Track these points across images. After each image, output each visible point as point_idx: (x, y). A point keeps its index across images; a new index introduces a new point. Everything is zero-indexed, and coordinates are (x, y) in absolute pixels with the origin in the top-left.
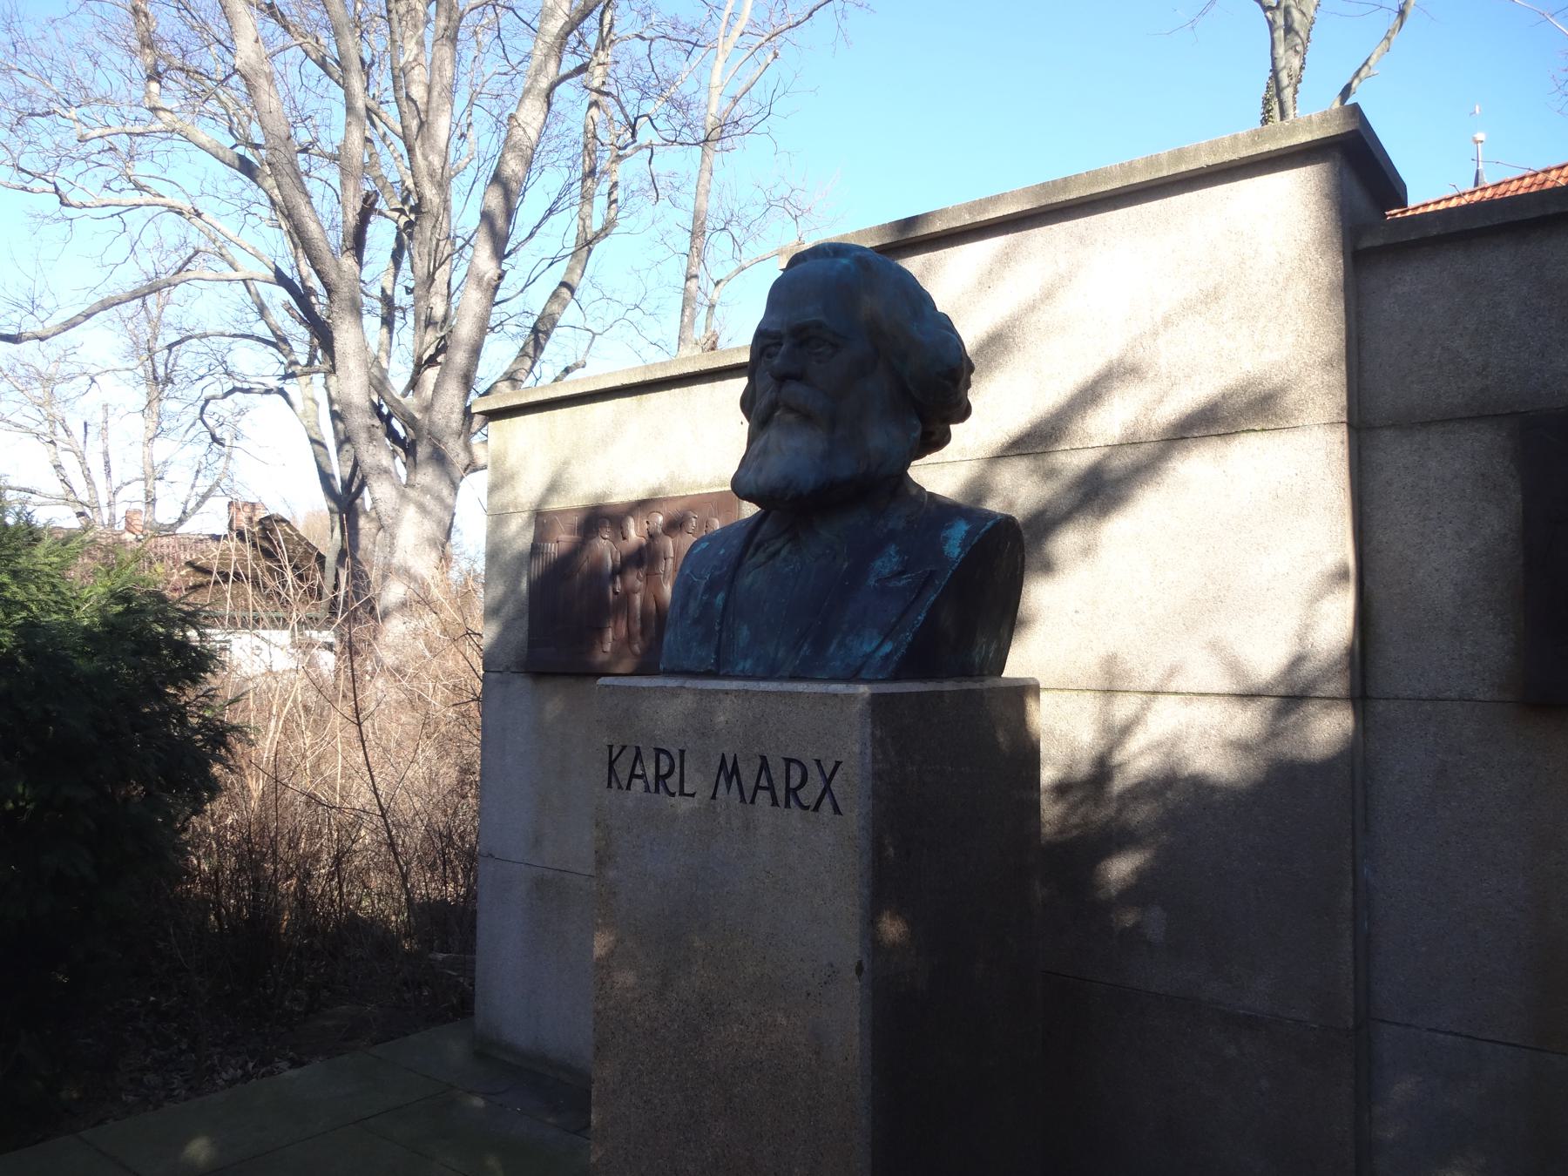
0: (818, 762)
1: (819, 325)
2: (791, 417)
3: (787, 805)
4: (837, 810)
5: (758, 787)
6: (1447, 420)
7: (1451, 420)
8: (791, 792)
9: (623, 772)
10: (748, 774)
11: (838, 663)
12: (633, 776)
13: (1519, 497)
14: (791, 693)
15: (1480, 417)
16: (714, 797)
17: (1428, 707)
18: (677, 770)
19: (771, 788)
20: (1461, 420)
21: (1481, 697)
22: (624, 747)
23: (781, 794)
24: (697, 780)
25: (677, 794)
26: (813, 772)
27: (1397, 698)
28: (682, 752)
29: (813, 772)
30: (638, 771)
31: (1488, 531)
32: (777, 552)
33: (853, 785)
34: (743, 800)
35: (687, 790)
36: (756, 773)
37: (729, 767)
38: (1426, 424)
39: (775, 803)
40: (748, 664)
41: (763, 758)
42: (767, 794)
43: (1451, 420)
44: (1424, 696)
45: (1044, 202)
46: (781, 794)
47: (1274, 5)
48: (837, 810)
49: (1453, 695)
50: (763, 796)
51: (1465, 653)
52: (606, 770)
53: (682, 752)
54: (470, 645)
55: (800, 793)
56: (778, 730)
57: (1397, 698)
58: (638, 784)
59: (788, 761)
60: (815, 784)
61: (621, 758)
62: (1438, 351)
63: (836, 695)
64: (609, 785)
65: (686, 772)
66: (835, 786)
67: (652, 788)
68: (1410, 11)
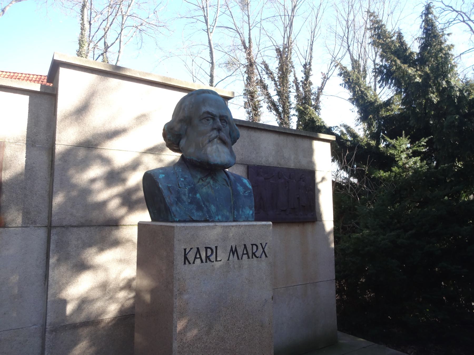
0: (261, 244)
3: (252, 258)
4: (266, 256)
5: (243, 254)
8: (254, 254)
9: (191, 257)
10: (240, 251)
11: (243, 216)
12: (196, 258)
14: (253, 225)
15: (242, 164)
16: (228, 260)
18: (214, 253)
19: (247, 254)
22: (191, 249)
23: (250, 255)
24: (222, 255)
25: (215, 261)
28: (216, 247)
30: (198, 256)
34: (238, 258)
35: (218, 259)
36: (243, 250)
37: (234, 249)
39: (249, 258)
40: (220, 217)
42: (246, 256)
45: (164, 82)
46: (250, 255)
48: (266, 256)
50: (245, 257)
52: (183, 258)
53: (216, 247)
55: (256, 254)
56: (249, 236)
58: (198, 261)
59: (252, 245)
61: (190, 253)
63: (266, 225)
64: (185, 263)
65: (218, 253)
66: (266, 250)
67: (204, 261)
68: (6, 11)
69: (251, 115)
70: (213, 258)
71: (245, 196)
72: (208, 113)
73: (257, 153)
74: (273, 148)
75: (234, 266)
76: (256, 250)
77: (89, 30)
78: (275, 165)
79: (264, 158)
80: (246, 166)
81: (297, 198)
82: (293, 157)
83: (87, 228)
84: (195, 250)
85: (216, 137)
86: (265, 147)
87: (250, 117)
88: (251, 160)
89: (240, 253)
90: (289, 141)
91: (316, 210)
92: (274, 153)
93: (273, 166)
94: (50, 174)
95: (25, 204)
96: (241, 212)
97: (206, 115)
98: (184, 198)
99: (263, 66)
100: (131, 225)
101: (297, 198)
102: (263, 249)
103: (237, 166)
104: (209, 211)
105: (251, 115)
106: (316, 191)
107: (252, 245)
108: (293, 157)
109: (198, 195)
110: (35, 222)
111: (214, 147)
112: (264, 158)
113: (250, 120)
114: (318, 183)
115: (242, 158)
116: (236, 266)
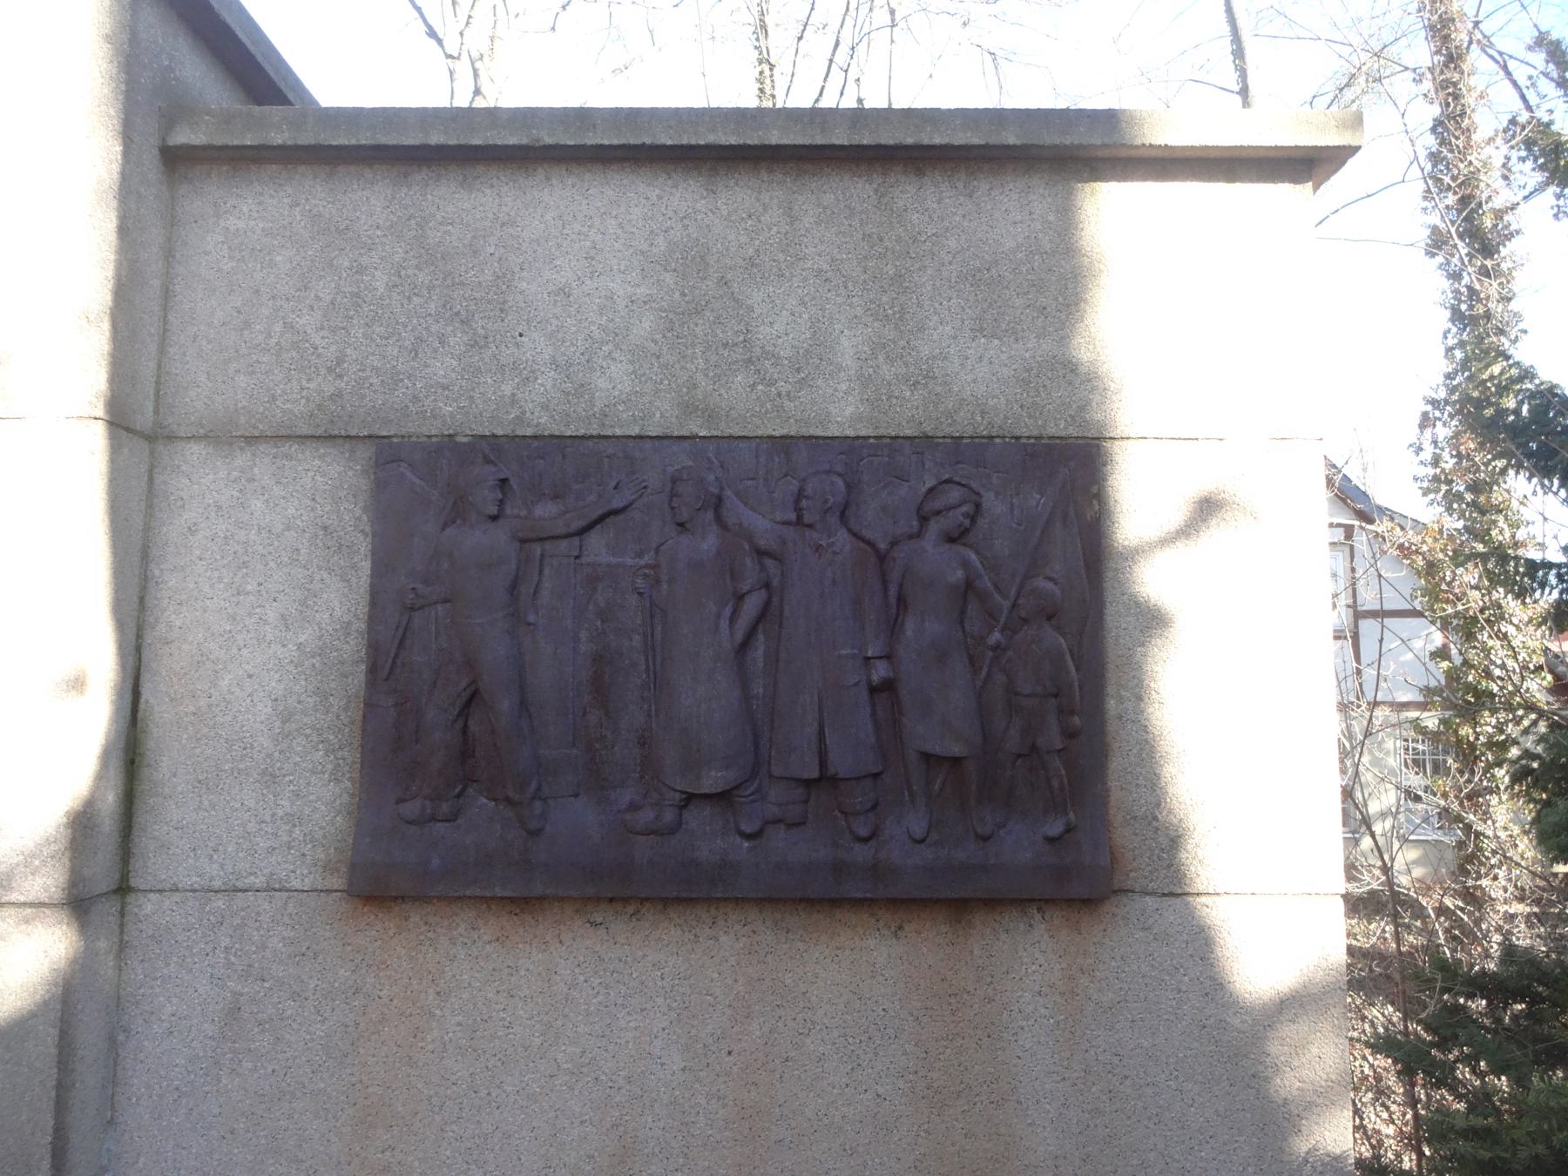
6: (283, 437)
7: (289, 437)
13: (366, 566)
17: (220, 902)
21: (296, 884)
27: (175, 889)
31: (326, 616)
38: (251, 440)
43: (289, 437)
44: (217, 884)
47: (456, 55)
49: (259, 881)
51: (280, 812)
57: (175, 889)
62: (278, 328)
69: (1466, 280)
73: (473, 344)
74: (642, 291)
76: (748, 831)
77: (1527, 194)
78: (663, 417)
79: (547, 380)
80: (365, 452)
81: (873, 690)
82: (848, 347)
86: (564, 292)
87: (1457, 292)
88: (415, 399)
91: (1115, 796)
93: (635, 431)
94: (139, 725)
95: (1356, 935)
99: (1539, 58)
100: (60, 1086)
101: (873, 690)
103: (288, 457)
105: (1463, 283)
106: (1116, 620)
108: (848, 347)
113: (1460, 301)
114: (1134, 553)
115: (338, 395)
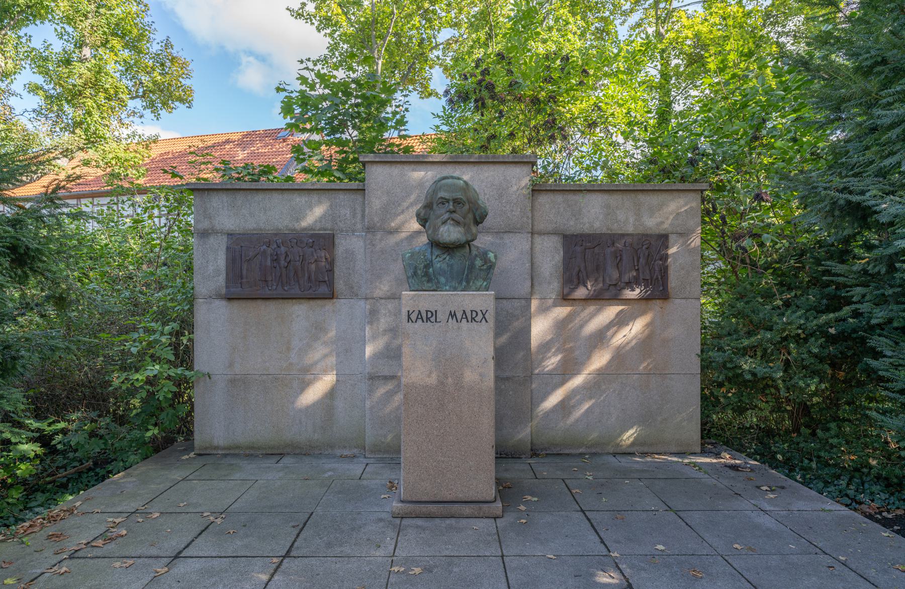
1: (461, 199)
2: (452, 222)
4: (487, 321)
8: (473, 319)
9: (413, 317)
10: (459, 316)
12: (417, 318)
20: (591, 299)
23: (470, 319)
26: (480, 313)
28: (436, 311)
29: (480, 313)
32: (445, 259)
33: (490, 316)
39: (468, 321)
40: (447, 288)
41: (464, 311)
46: (470, 319)
48: (487, 321)
50: (464, 321)
53: (436, 311)
54: (885, 412)
59: (472, 311)
60: (480, 316)
66: (486, 316)
67: (425, 321)
70: (433, 319)
71: (481, 270)
72: (442, 198)
75: (453, 327)
79: (587, 225)
82: (631, 220)
83: (393, 300)
84: (417, 312)
85: (449, 219)
89: (459, 317)
90: (627, 201)
92: (601, 217)
96: (471, 284)
97: (440, 201)
98: (419, 272)
102: (484, 315)
104: (438, 282)
107: (472, 311)
109: (431, 270)
110: (357, 295)
111: (447, 227)
112: (587, 225)
116: (455, 327)
